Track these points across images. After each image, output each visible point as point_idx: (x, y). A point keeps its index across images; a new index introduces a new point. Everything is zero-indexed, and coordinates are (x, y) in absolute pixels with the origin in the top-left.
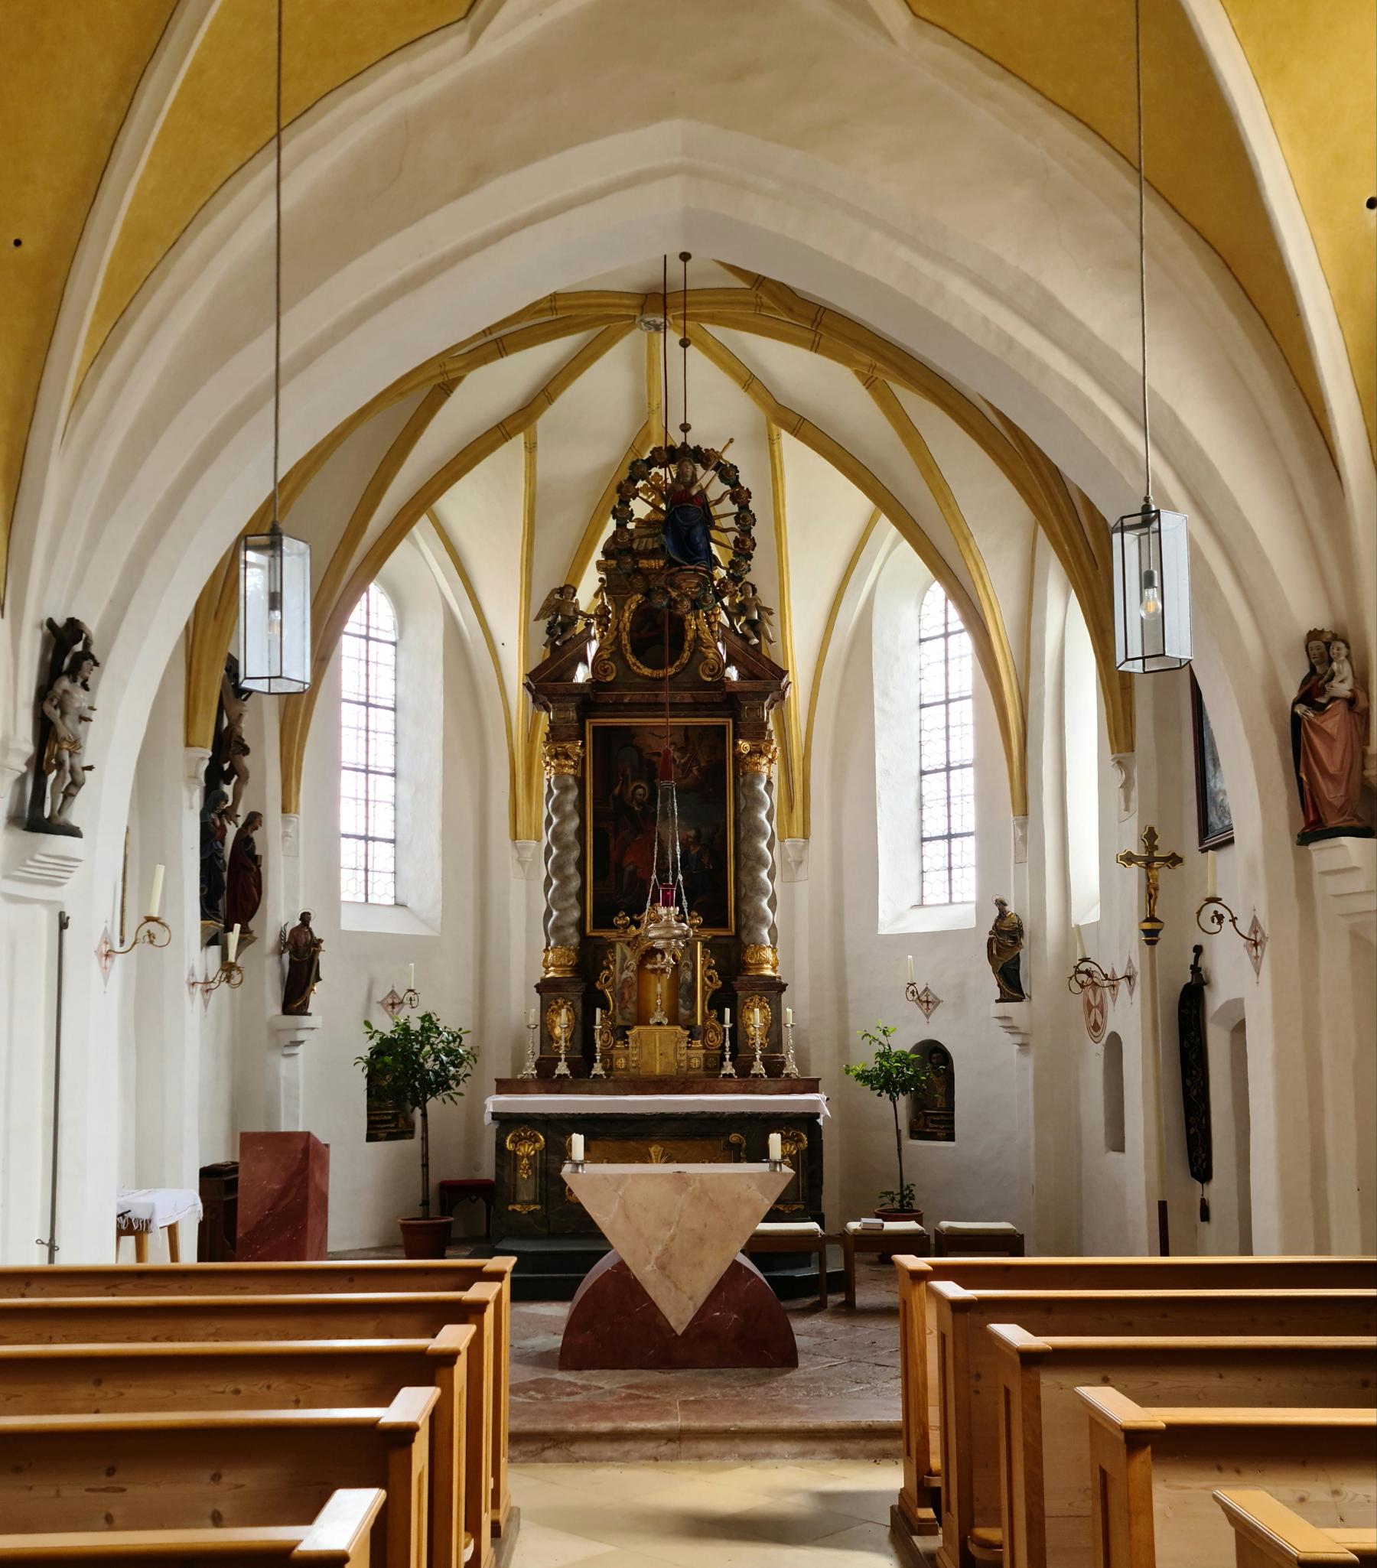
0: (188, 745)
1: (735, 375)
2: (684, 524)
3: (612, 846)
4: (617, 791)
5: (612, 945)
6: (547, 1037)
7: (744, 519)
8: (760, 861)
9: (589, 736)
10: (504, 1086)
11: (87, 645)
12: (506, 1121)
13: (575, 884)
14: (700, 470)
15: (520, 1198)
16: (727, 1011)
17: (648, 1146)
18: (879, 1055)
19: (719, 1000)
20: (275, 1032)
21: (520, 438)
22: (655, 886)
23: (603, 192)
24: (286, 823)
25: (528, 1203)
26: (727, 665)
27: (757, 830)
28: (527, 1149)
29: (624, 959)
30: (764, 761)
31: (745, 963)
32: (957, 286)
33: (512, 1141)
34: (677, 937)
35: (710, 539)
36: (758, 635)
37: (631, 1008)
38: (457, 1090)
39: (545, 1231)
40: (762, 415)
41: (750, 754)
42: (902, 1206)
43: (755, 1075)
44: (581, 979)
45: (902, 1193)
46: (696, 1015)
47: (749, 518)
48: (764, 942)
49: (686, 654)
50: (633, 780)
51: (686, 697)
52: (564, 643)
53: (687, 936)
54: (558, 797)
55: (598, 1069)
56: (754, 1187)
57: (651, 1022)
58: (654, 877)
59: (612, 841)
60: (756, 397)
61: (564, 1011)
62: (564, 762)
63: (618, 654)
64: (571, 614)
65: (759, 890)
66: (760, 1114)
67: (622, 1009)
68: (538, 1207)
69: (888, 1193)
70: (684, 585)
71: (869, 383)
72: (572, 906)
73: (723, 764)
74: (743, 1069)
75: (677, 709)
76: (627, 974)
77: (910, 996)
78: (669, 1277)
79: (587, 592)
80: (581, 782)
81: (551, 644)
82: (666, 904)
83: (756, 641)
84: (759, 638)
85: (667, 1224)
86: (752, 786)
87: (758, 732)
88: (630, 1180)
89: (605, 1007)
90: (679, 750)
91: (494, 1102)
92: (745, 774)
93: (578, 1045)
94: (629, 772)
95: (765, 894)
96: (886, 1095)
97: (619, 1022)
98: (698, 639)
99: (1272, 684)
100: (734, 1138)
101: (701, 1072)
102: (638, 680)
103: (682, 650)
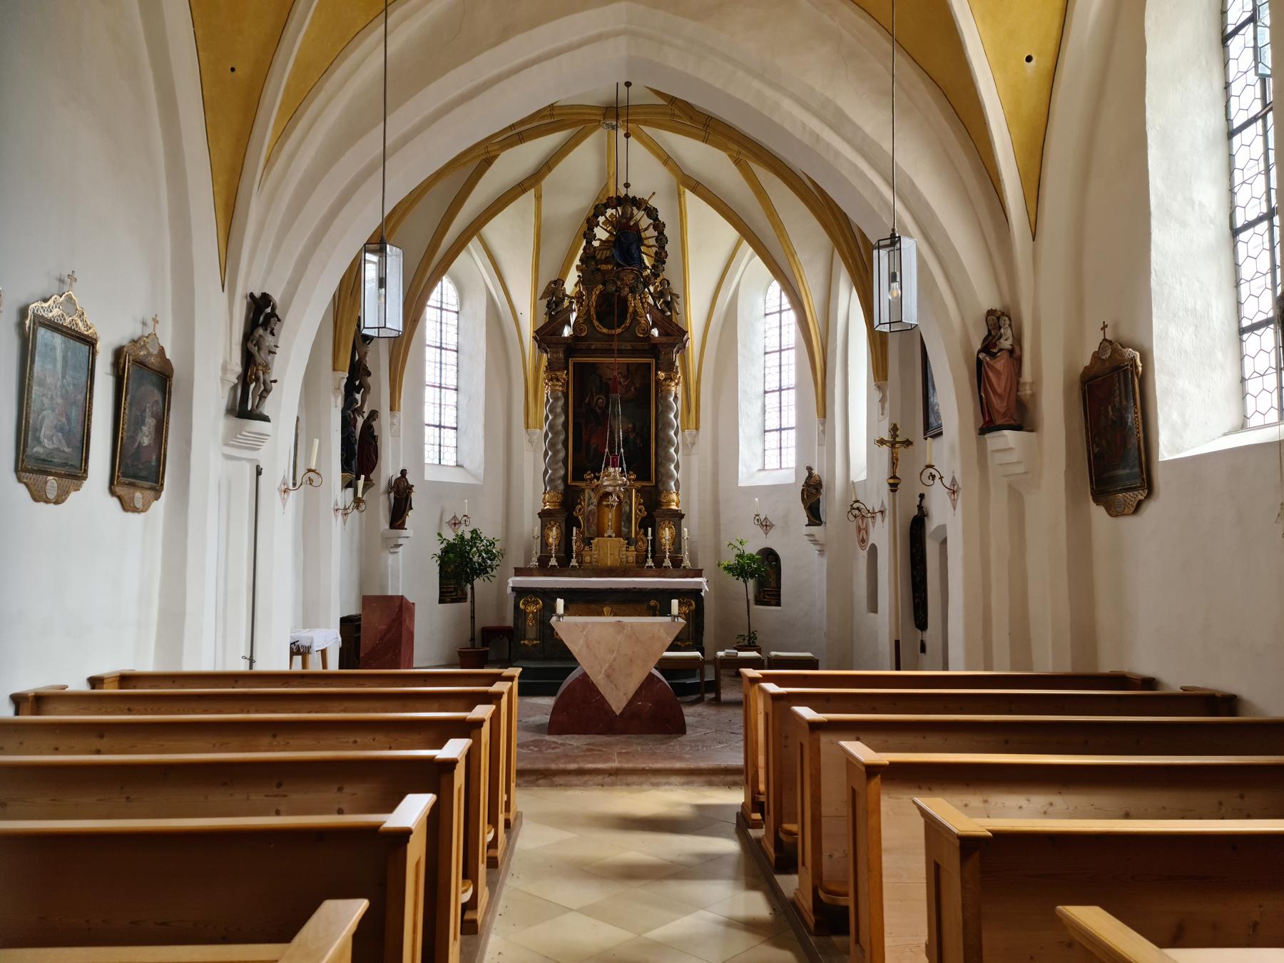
0: (334, 370)
1: (659, 156)
2: (626, 241)
5: (583, 490)
9: (571, 368)
10: (519, 572)
11: (273, 309)
12: (520, 592)
20: (385, 539)
21: (531, 193)
23: (580, 45)
24: (392, 416)
27: (668, 425)
28: (532, 608)
32: (787, 104)
35: (640, 252)
37: (594, 527)
40: (674, 180)
44: (565, 511)
49: (628, 321)
55: (574, 562)
60: (671, 169)
71: (737, 162)
74: (659, 563)
75: (622, 353)
76: (592, 507)
79: (571, 284)
80: (566, 395)
81: (549, 314)
82: (614, 466)
86: (666, 398)
87: (670, 367)
89: (579, 526)
91: (513, 581)
97: (587, 535)
98: (635, 312)
99: (967, 340)
100: (653, 603)
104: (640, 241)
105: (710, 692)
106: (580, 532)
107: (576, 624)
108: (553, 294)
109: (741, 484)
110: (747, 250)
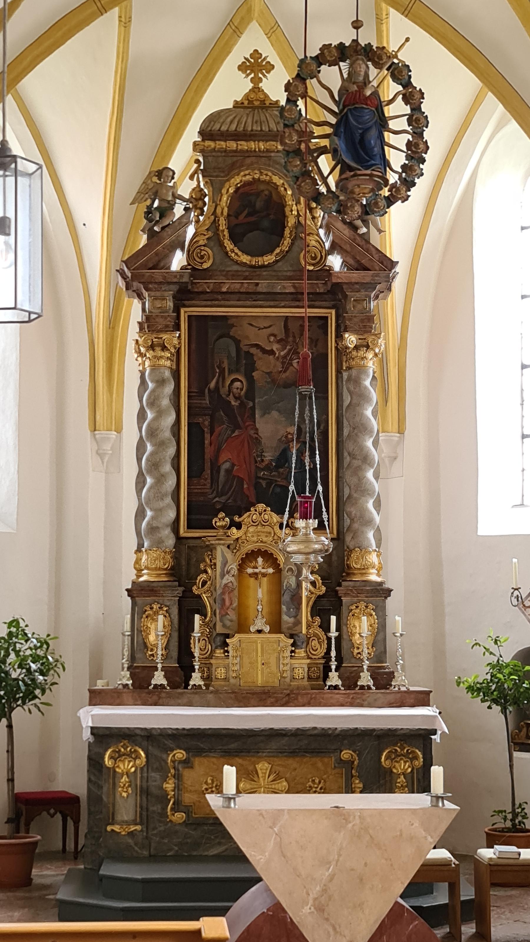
3: (207, 442)
4: (212, 385)
5: (211, 549)
6: (138, 645)
7: (417, 120)
8: (366, 459)
9: (184, 325)
10: (97, 697)
12: (103, 737)
13: (171, 482)
14: (373, 72)
15: (118, 818)
16: (333, 619)
17: (254, 764)
18: (492, 666)
19: (328, 606)
22: (293, 497)
25: (128, 823)
26: (330, 252)
27: (361, 428)
28: (126, 766)
29: (225, 563)
30: (370, 355)
31: (349, 567)
33: (111, 757)
34: (315, 552)
35: (383, 143)
36: (366, 223)
37: (232, 615)
38: (44, 699)
39: (146, 853)
41: (356, 348)
42: (514, 825)
43: (362, 687)
44: (179, 585)
45: (514, 810)
46: (300, 623)
47: (423, 120)
48: (370, 545)
49: (287, 242)
50: (231, 372)
51: (288, 287)
52: (163, 228)
53: (327, 551)
54: (153, 391)
55: (196, 679)
56: (416, 824)
57: (252, 629)
58: (292, 487)
59: (207, 436)
61: (161, 618)
62: (160, 353)
63: (215, 239)
64: (170, 198)
65: (363, 489)
66: (374, 730)
67: (222, 616)
68: (138, 828)
69: (501, 812)
70: (357, 190)
72: (168, 506)
73: (325, 356)
74: (350, 681)
75: (273, 298)
76: (228, 579)
77: (515, 602)
78: (327, 919)
80: (176, 374)
82: (305, 516)
83: (364, 230)
84: (368, 227)
85: (325, 863)
86: (357, 381)
87: (366, 325)
88: (286, 816)
89: (204, 614)
90: (278, 342)
91: (91, 716)
92: (349, 368)
93: (175, 654)
94: (226, 365)
95: (371, 495)
96: (496, 709)
97: (219, 629)
100: (346, 754)
101: (305, 682)
102: (236, 268)
103: (282, 235)
104: (382, 123)
105: (466, 920)
106: (204, 624)
107: (260, 813)
108: (156, 195)
109: (481, 532)
110: (494, 108)
